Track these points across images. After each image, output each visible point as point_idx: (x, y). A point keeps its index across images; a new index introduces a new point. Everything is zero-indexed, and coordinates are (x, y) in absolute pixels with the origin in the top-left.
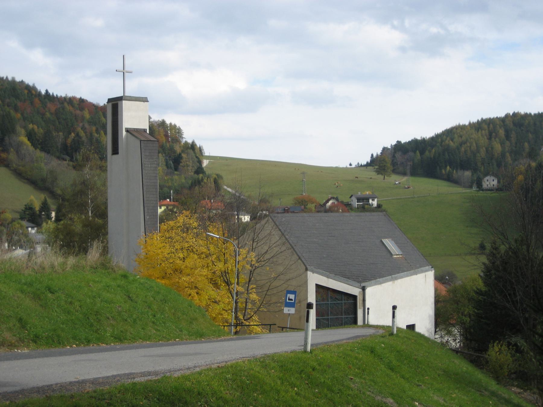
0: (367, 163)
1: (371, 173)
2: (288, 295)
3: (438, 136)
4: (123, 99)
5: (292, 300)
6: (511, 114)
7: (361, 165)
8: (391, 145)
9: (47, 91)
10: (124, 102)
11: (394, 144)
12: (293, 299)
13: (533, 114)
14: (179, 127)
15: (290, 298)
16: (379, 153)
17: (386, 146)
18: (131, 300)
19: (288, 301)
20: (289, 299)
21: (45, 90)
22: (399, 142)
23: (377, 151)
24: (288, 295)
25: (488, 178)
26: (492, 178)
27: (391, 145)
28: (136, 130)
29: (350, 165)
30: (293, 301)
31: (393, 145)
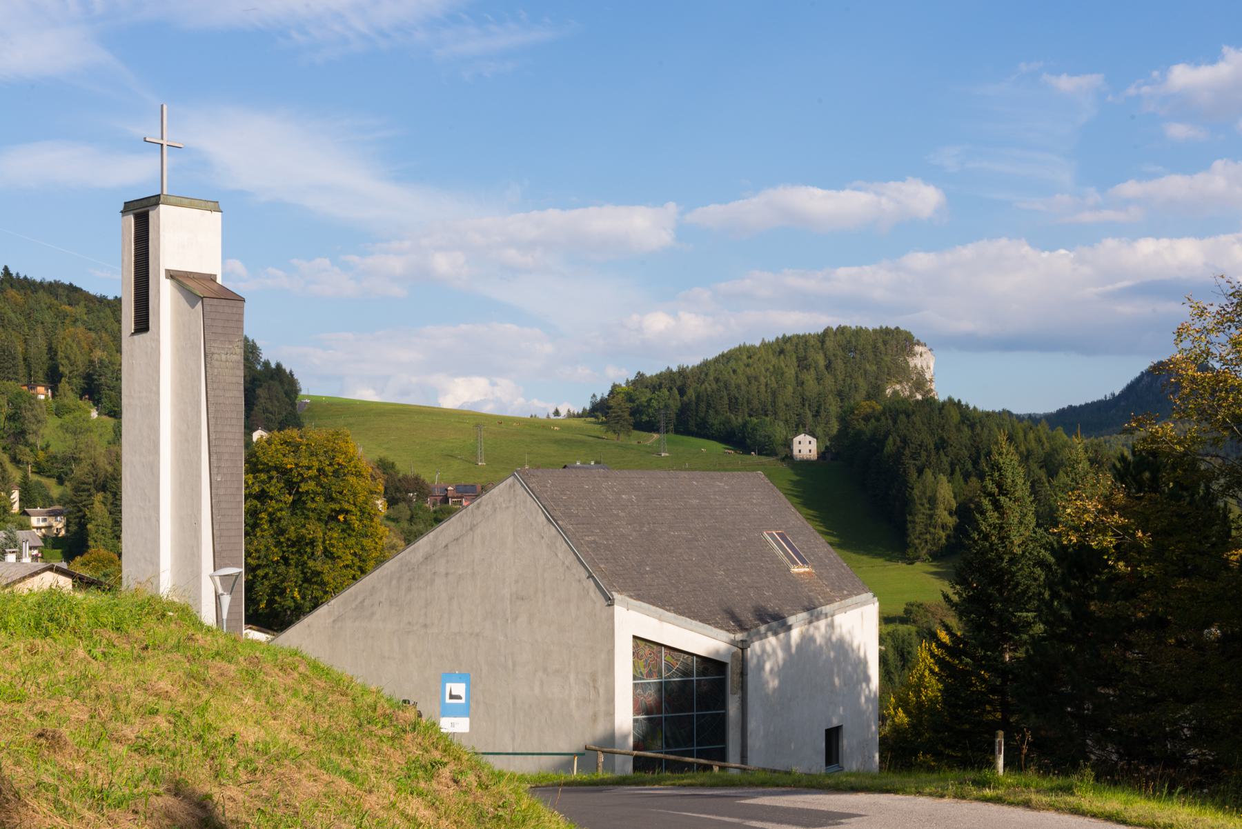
0: (584, 410)
1: (588, 424)
2: (448, 686)
3: (706, 364)
4: (162, 200)
5: (459, 697)
6: (835, 329)
7: (574, 414)
8: (627, 380)
9: (18, 274)
10: (163, 208)
11: (633, 378)
12: (463, 695)
13: (871, 329)
14: (975, 407)
15: (453, 693)
16: (606, 395)
17: (617, 383)
18: (117, 741)
19: (448, 701)
20: (452, 697)
21: (3, 267)
22: (640, 376)
23: (603, 391)
24: (448, 686)
25: (801, 437)
26: (809, 438)
27: (627, 380)
28: (192, 276)
29: (557, 413)
30: (463, 701)
31: (630, 381)
